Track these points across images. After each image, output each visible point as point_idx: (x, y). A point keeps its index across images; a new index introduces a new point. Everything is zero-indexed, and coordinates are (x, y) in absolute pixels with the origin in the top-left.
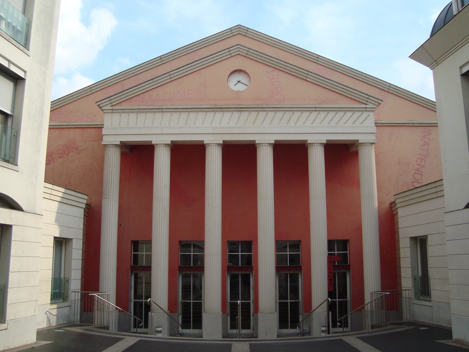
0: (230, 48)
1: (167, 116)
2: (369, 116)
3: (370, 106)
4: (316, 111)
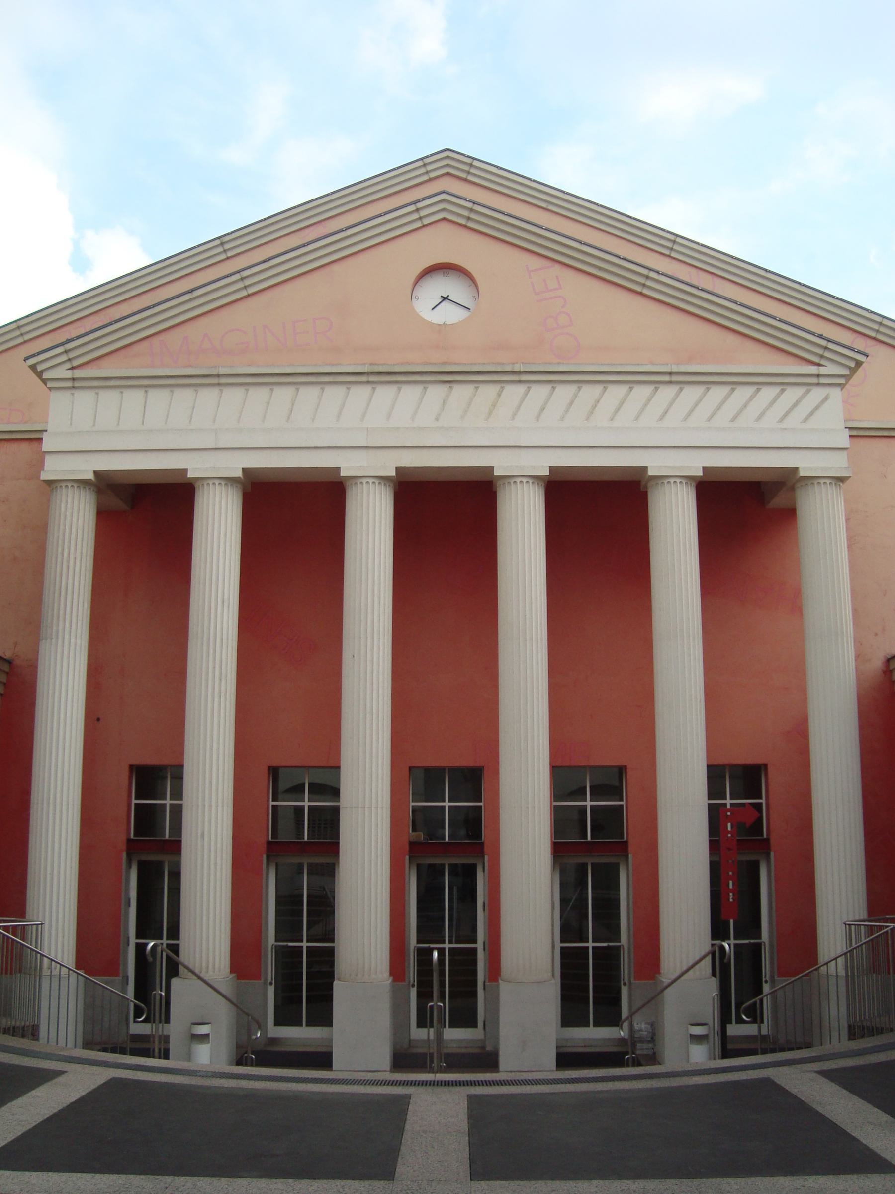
0: (419, 201)
1: (233, 395)
2: (826, 398)
3: (829, 369)
4: (670, 382)
